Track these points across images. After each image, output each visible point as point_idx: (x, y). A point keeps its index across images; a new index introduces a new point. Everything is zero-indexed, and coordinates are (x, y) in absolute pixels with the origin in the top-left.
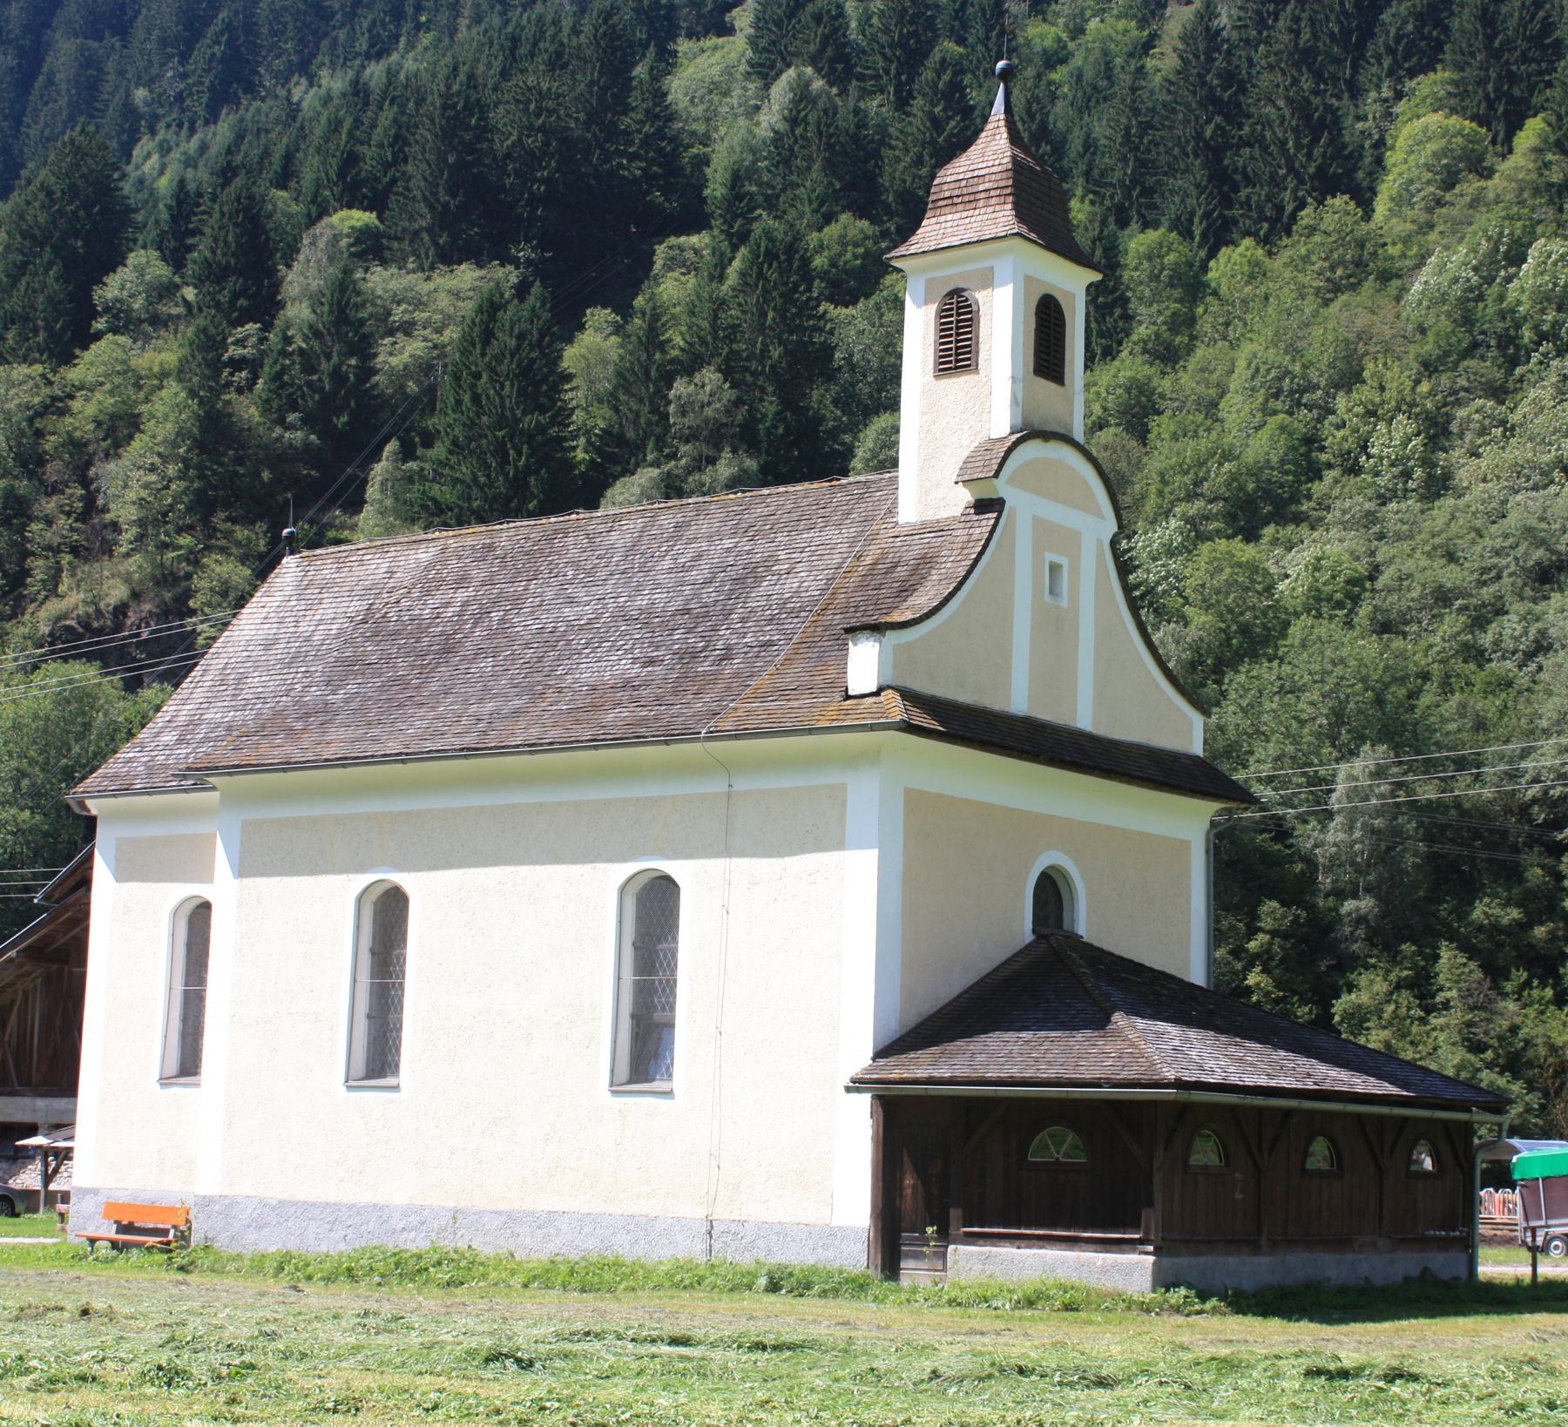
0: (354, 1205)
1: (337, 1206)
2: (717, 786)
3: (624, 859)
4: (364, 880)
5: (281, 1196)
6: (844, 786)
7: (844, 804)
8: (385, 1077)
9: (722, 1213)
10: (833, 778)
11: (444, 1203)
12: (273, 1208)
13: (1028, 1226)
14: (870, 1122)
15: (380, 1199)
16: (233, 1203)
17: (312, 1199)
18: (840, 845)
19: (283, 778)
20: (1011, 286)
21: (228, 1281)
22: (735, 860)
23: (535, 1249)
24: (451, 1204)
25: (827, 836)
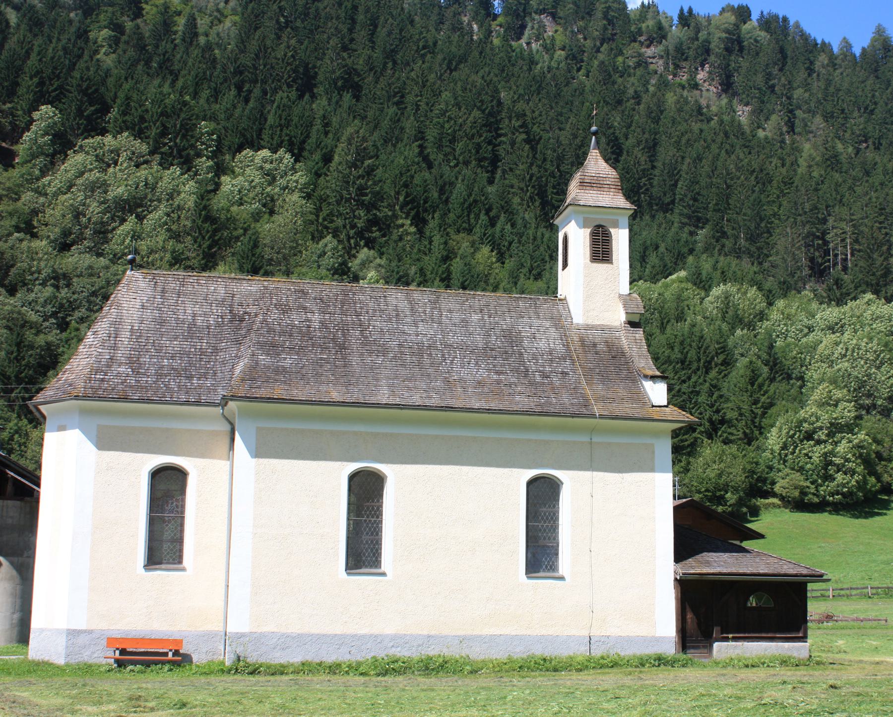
0: (356, 635)
1: (343, 637)
2: (585, 439)
3: (530, 467)
4: (353, 467)
5: (299, 632)
6: (653, 445)
7: (653, 452)
8: (538, 572)
9: (596, 632)
10: (648, 441)
11: (420, 633)
12: (294, 638)
13: (749, 633)
14: (673, 591)
15: (375, 631)
16: (262, 635)
17: (324, 632)
18: (652, 470)
19: (122, 407)
20: (573, 222)
21: (337, 677)
22: (595, 473)
23: (499, 654)
24: (425, 633)
25: (649, 467)
